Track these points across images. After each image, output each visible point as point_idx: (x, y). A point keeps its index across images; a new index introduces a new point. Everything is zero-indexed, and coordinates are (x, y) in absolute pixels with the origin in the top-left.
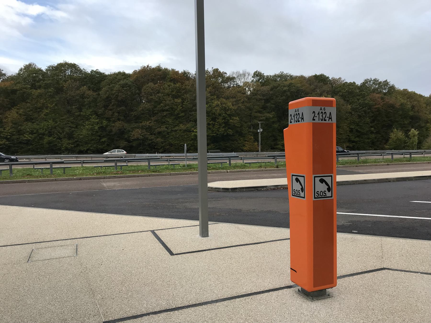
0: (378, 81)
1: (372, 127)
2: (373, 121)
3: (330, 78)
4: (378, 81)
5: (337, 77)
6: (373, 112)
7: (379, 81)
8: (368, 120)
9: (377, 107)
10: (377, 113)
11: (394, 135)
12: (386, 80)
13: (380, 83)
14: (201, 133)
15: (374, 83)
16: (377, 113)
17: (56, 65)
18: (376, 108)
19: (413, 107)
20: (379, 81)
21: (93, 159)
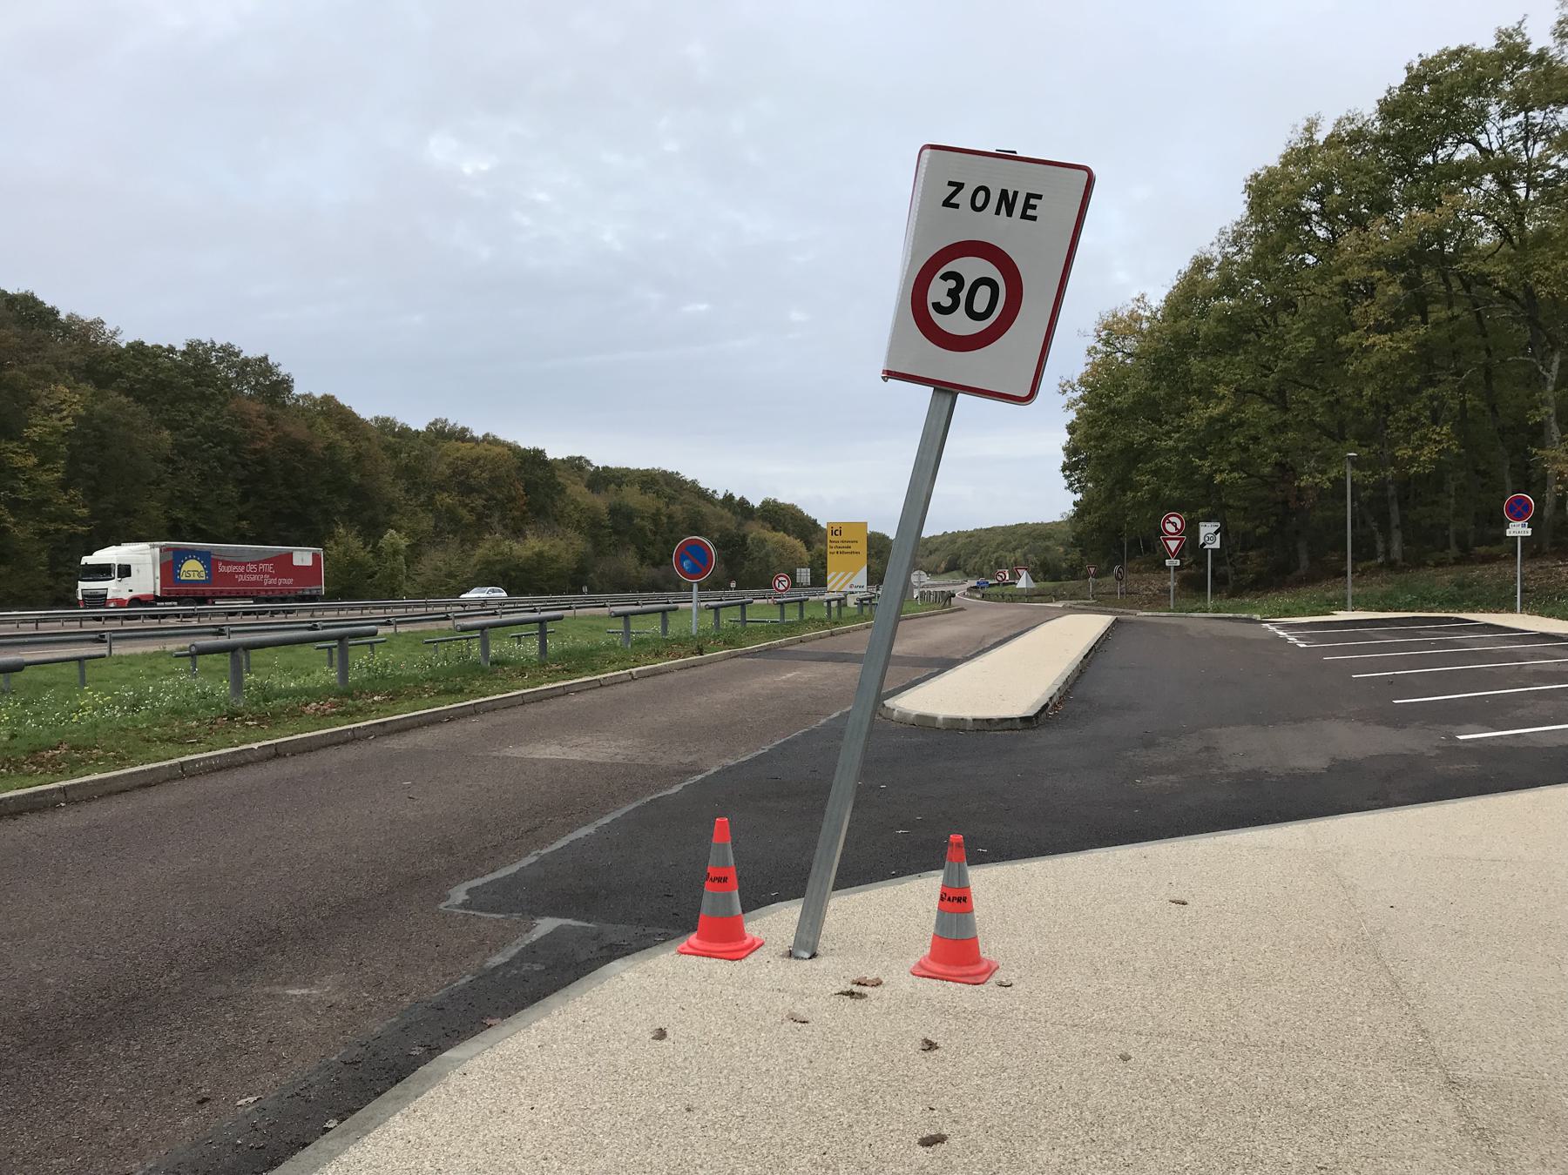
0: (237, 355)
1: (241, 518)
2: (245, 497)
3: (63, 316)
4: (237, 355)
5: (87, 315)
6: (244, 466)
7: (242, 356)
8: (231, 491)
9: (258, 445)
10: (259, 469)
11: (341, 548)
12: (266, 358)
13: (246, 362)
14: (1350, 600)
15: (221, 360)
16: (259, 469)
17: (124, 341)
18: (256, 451)
19: (358, 458)
20: (242, 356)
21: (153, 623)
